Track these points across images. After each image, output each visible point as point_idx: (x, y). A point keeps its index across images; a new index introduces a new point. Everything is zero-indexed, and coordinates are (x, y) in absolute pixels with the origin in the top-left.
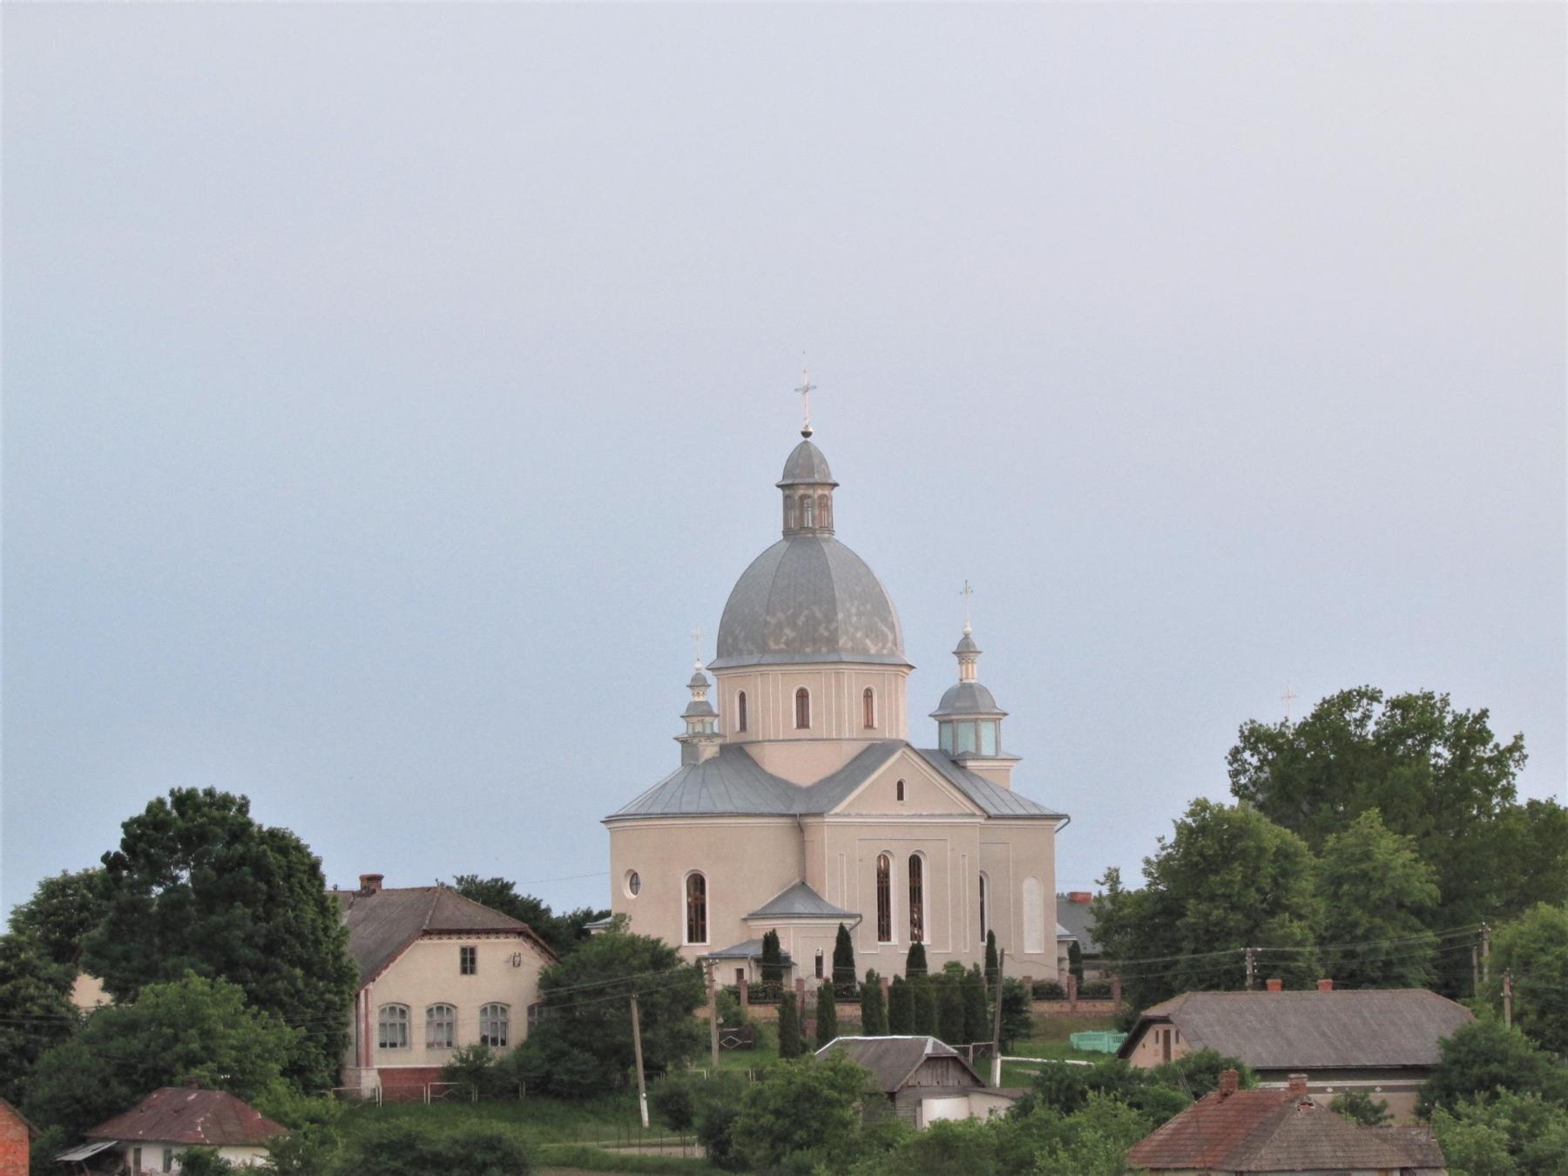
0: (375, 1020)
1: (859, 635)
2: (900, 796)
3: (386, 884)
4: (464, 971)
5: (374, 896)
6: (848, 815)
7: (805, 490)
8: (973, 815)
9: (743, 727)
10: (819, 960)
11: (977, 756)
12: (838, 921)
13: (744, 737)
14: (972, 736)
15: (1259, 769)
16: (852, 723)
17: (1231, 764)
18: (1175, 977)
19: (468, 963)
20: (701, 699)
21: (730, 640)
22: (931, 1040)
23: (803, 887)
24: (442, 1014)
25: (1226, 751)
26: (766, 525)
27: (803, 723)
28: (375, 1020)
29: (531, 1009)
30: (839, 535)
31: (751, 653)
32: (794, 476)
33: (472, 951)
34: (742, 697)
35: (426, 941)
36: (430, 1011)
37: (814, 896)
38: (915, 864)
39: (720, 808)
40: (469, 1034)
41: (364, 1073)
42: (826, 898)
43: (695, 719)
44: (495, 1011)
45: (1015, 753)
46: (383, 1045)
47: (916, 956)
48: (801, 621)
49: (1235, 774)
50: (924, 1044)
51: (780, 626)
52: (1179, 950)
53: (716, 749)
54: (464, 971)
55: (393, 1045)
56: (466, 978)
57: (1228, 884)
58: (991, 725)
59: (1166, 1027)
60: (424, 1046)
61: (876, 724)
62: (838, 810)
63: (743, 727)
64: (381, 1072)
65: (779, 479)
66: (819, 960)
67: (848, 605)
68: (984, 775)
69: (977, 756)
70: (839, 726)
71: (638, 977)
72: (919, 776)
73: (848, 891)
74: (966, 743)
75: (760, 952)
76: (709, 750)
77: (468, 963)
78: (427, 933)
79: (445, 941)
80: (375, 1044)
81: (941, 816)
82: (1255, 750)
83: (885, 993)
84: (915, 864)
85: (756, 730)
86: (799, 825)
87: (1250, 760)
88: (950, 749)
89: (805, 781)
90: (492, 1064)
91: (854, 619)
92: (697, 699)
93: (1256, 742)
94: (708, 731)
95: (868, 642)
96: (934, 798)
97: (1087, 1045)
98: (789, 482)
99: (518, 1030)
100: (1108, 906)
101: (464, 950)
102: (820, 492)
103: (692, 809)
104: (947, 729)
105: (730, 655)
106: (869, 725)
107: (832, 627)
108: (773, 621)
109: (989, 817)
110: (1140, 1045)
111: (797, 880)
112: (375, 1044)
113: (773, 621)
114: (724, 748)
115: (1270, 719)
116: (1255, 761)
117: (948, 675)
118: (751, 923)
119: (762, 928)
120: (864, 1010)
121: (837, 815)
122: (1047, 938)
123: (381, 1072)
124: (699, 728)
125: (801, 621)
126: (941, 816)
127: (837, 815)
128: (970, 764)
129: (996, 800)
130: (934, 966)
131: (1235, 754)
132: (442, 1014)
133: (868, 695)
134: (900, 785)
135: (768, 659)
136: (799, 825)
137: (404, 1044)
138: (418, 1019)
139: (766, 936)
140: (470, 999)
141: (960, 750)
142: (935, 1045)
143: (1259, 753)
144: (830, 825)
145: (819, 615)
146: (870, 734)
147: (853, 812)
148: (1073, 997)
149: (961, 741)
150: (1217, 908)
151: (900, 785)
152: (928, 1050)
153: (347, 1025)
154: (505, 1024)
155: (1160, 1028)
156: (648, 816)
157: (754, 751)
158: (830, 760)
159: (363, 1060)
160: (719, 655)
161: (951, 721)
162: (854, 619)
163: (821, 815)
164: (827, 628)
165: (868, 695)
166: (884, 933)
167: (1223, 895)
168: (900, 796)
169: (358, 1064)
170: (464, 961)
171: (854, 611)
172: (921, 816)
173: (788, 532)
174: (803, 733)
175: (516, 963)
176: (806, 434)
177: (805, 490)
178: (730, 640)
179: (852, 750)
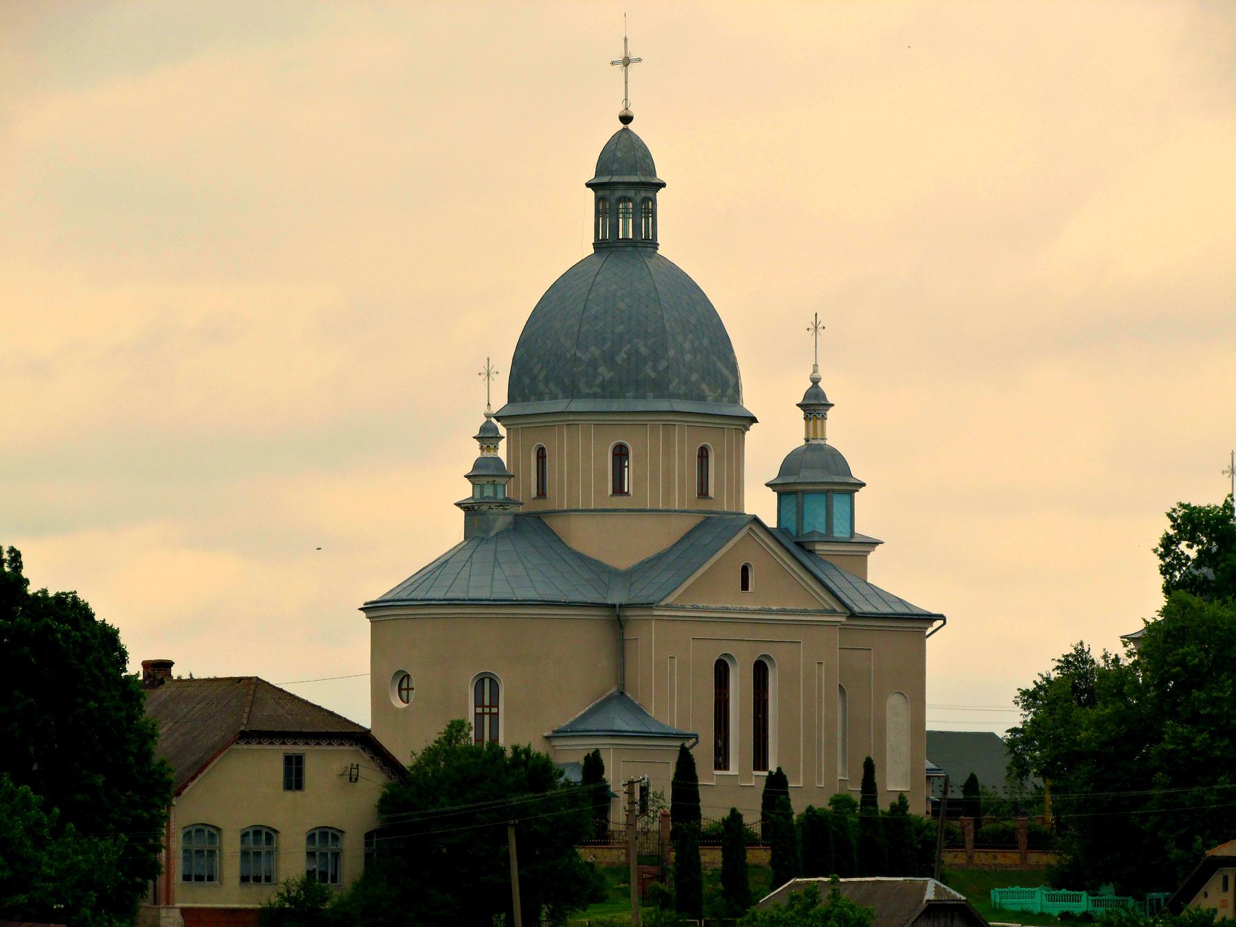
0: (177, 845)
1: (694, 377)
2: (745, 586)
3: (175, 672)
4: (288, 787)
5: (162, 689)
6: (683, 608)
7: (625, 184)
9: (542, 493)
11: (829, 539)
12: (679, 743)
13: (541, 506)
14: (822, 512)
15: (1198, 563)
16: (682, 495)
17: (1162, 557)
18: (1145, 818)
19: (294, 777)
20: (491, 454)
21: (526, 381)
22: (932, 883)
23: (620, 697)
24: (261, 839)
25: (1156, 542)
26: (571, 234)
27: (619, 489)
28: (177, 845)
29: (369, 836)
30: (665, 249)
31: (554, 397)
32: (611, 173)
33: (299, 759)
34: (541, 454)
35: (243, 746)
36: (245, 835)
38: (760, 671)
39: (521, 594)
40: (292, 865)
41: (163, 913)
43: (484, 480)
44: (324, 839)
45: (873, 534)
46: (187, 878)
48: (620, 357)
49: (1165, 570)
50: (923, 888)
51: (594, 363)
52: (1151, 786)
53: (510, 519)
54: (288, 787)
55: (199, 878)
57: (1214, 702)
58: (821, 499)
60: (238, 880)
61: (711, 493)
62: (669, 600)
63: (542, 493)
64: (185, 912)
65: (590, 175)
67: (680, 338)
68: (830, 559)
69: (829, 539)
70: (668, 491)
71: (514, 800)
72: (769, 563)
73: (677, 703)
74: (815, 521)
76: (501, 522)
77: (294, 777)
78: (248, 736)
81: (794, 612)
82: (1193, 540)
83: (799, 835)
84: (760, 671)
85: (558, 497)
86: (617, 620)
87: (1188, 552)
88: (793, 527)
89: (623, 563)
90: (327, 906)
91: (688, 357)
92: (486, 454)
93: (1194, 529)
94: (500, 496)
96: (779, 591)
98: (605, 179)
99: (352, 864)
100: (157, 800)
101: (288, 760)
102: (643, 194)
103: (483, 594)
104: (791, 502)
105: (526, 399)
106: (703, 493)
107: (663, 364)
108: (585, 357)
109: (853, 615)
113: (585, 357)
114: (519, 520)
115: (78, 595)
116: (1193, 553)
118: (556, 743)
120: (725, 856)
121: (668, 607)
122: (914, 772)
123: (185, 912)
124: (489, 492)
125: (620, 357)
126: (794, 612)
127: (668, 607)
128: (818, 547)
129: (856, 596)
130: (798, 807)
131: (1168, 542)
132: (261, 839)
133: (703, 454)
134: (745, 570)
135: (577, 405)
136: (617, 620)
137: (211, 878)
138: (231, 846)
139: (587, 758)
140: (294, 819)
141: (807, 529)
143: (1200, 542)
144: (659, 619)
145: (643, 350)
146: (704, 505)
147: (688, 605)
148: (969, 843)
149: (808, 519)
150: (1201, 731)
151: (745, 570)
152: (930, 895)
153: (157, 849)
154: (336, 855)
156: (428, 603)
157: (556, 524)
158: (652, 538)
159: (163, 897)
160: (511, 398)
161: (795, 493)
162: (688, 357)
163: (648, 606)
164: (655, 369)
165: (703, 454)
166: (721, 760)
167: (1209, 716)
168: (745, 586)
169: (156, 902)
170: (300, 772)
171: (687, 346)
172: (769, 611)
173: (598, 245)
174: (619, 502)
176: (626, 119)
177: (625, 184)
178: (526, 381)
179: (683, 525)
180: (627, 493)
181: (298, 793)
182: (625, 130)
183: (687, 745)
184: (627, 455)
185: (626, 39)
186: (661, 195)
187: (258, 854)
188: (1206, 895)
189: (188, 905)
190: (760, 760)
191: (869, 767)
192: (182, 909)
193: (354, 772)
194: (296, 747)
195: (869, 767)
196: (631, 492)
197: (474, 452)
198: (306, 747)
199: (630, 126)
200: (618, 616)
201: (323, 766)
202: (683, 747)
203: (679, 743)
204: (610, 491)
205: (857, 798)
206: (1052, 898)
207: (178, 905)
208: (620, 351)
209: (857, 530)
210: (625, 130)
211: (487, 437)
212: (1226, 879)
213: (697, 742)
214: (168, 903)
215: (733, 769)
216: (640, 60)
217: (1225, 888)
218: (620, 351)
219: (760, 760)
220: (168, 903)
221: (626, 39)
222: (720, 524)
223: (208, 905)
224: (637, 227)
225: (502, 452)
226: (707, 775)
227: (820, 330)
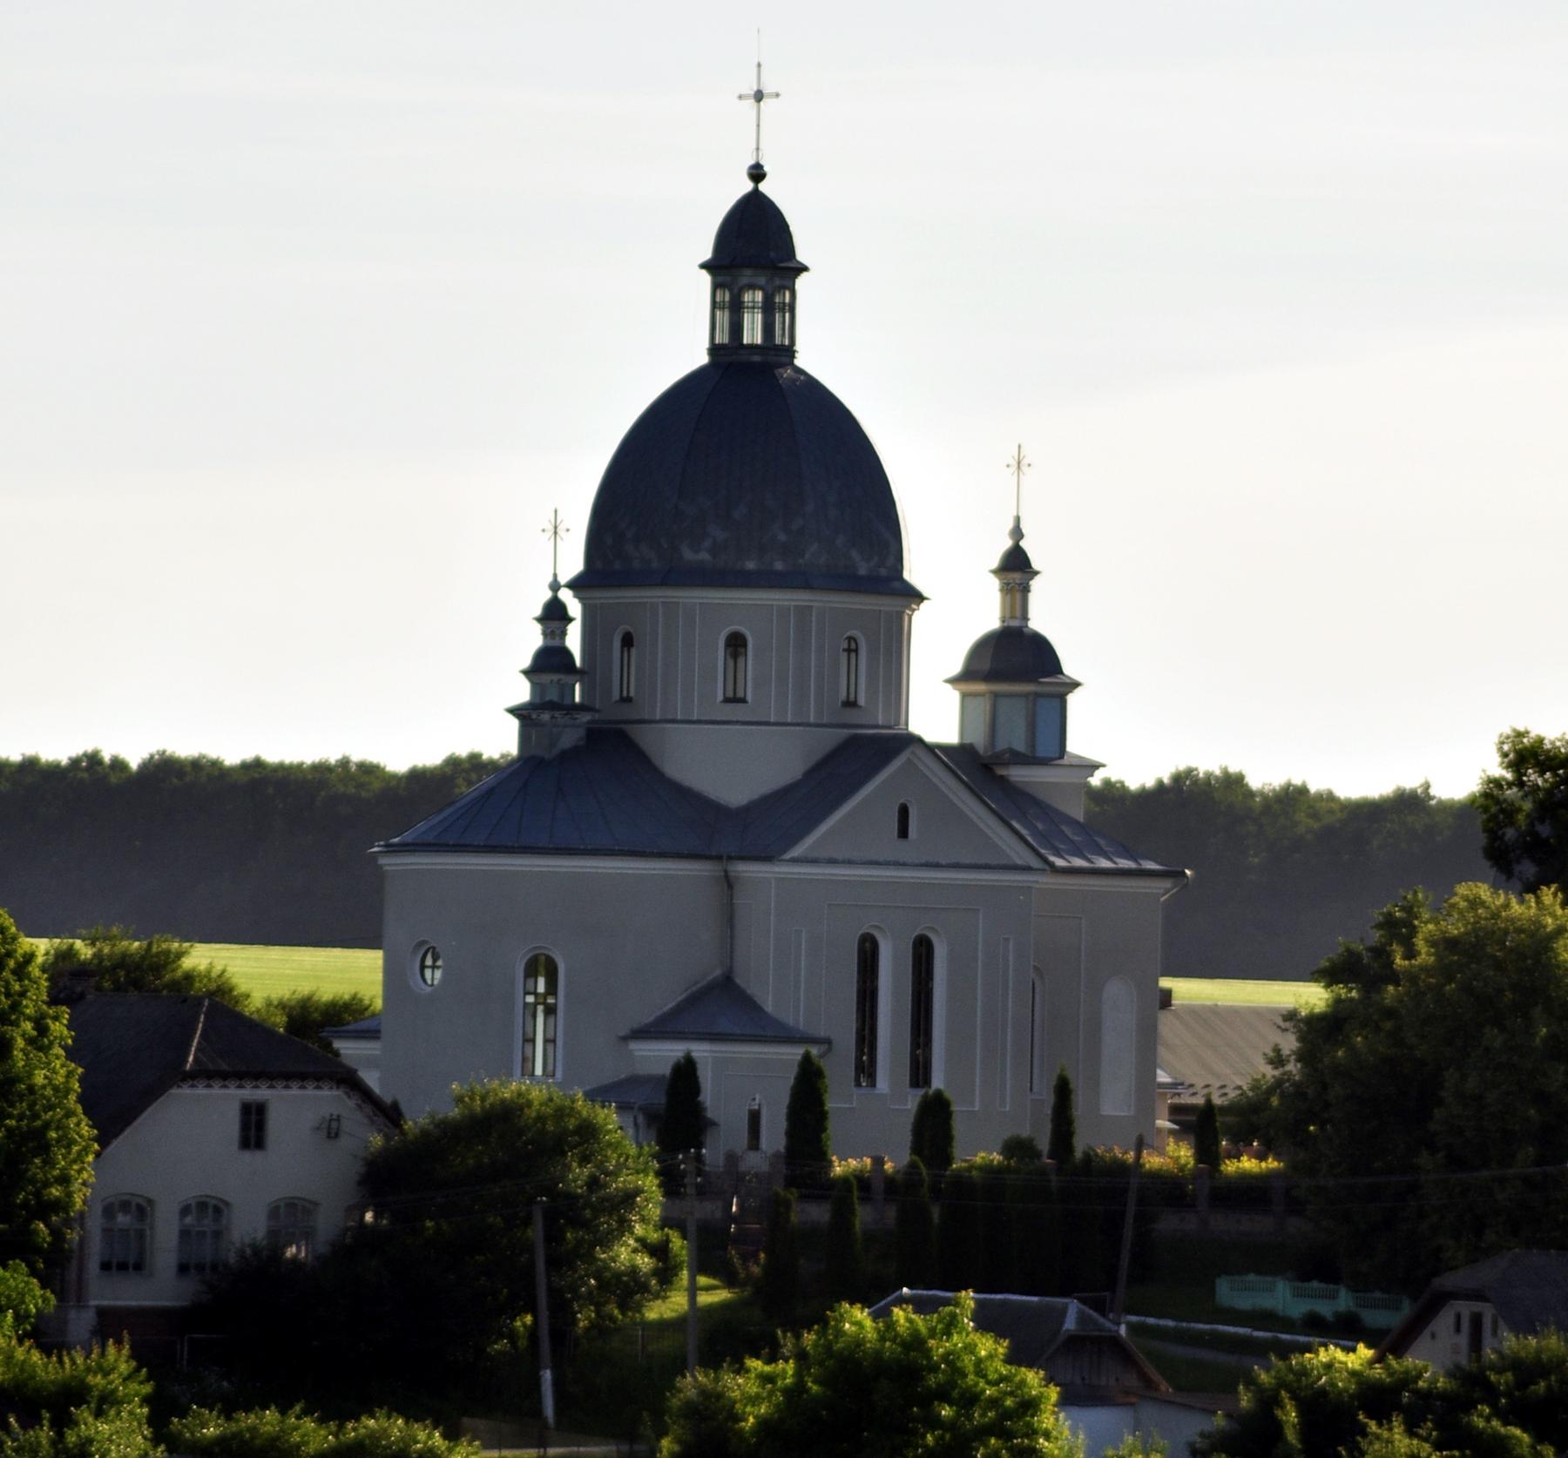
2: (903, 833)
8: (1027, 869)
10: (755, 1118)
12: (795, 1053)
30: (801, 361)
37: (748, 1004)
38: (923, 952)
41: (72, 1314)
42: (769, 1007)
46: (106, 1266)
47: (934, 1122)
50: (1063, 1313)
53: (582, 732)
55: (123, 1267)
56: (248, 1156)
59: (1477, 1306)
66: (755, 1118)
75: (660, 1099)
79: (217, 1091)
80: (93, 1266)
84: (923, 952)
95: (854, 554)
97: (1244, 1302)
110: (1427, 1333)
111: (718, 972)
112: (93, 1266)
117: (984, 613)
119: (661, 1055)
127: (794, 861)
128: (1018, 774)
130: (977, 1151)
134: (904, 812)
137: (138, 1267)
142: (1082, 1319)
151: (904, 812)
155: (1466, 1308)
157: (646, 738)
166: (866, 1070)
168: (903, 833)
170: (245, 1127)
173: (714, 350)
175: (331, 1130)
177: (754, 249)
180: (743, 701)
181: (258, 1155)
182: (756, 192)
183: (814, 1051)
184: (745, 646)
185: (759, 65)
186: (801, 282)
187: (202, 1234)
188: (1433, 1336)
189: (106, 1303)
190: (920, 1072)
191: (1063, 1091)
192: (97, 1307)
193: (334, 1125)
194: (259, 1092)
195: (1063, 1091)
196: (749, 698)
197: (534, 639)
198: (269, 1092)
199: (762, 187)
200: (726, 872)
201: (295, 1109)
202: (807, 1058)
203: (795, 1053)
204: (720, 697)
205: (1044, 1144)
206: (1298, 1294)
207: (93, 1303)
208: (745, 477)
209: (1069, 748)
210: (756, 192)
211: (554, 615)
212: (1458, 1317)
213: (830, 1050)
214: (79, 1299)
215: (883, 1083)
216: (777, 95)
217: (1458, 1329)
218: (745, 477)
219: (920, 1072)
220: (79, 1299)
221: (759, 65)
222: (870, 747)
223: (134, 1303)
224: (768, 329)
225: (573, 639)
226: (839, 1098)
227: (1024, 468)
